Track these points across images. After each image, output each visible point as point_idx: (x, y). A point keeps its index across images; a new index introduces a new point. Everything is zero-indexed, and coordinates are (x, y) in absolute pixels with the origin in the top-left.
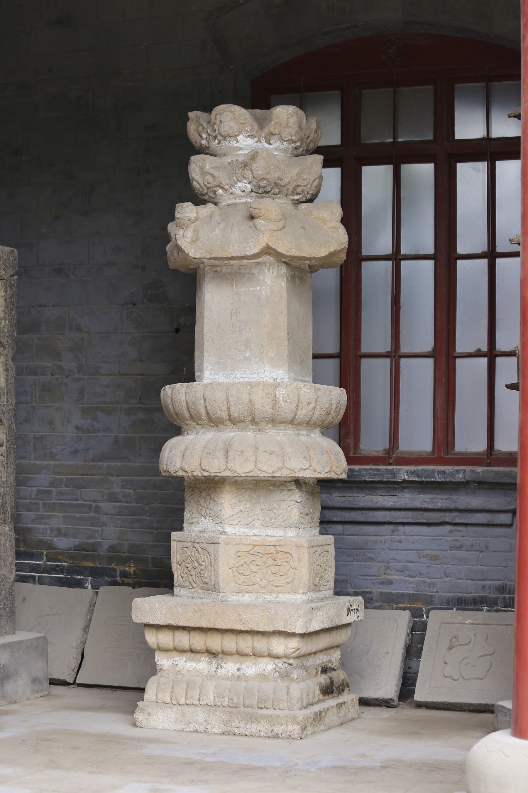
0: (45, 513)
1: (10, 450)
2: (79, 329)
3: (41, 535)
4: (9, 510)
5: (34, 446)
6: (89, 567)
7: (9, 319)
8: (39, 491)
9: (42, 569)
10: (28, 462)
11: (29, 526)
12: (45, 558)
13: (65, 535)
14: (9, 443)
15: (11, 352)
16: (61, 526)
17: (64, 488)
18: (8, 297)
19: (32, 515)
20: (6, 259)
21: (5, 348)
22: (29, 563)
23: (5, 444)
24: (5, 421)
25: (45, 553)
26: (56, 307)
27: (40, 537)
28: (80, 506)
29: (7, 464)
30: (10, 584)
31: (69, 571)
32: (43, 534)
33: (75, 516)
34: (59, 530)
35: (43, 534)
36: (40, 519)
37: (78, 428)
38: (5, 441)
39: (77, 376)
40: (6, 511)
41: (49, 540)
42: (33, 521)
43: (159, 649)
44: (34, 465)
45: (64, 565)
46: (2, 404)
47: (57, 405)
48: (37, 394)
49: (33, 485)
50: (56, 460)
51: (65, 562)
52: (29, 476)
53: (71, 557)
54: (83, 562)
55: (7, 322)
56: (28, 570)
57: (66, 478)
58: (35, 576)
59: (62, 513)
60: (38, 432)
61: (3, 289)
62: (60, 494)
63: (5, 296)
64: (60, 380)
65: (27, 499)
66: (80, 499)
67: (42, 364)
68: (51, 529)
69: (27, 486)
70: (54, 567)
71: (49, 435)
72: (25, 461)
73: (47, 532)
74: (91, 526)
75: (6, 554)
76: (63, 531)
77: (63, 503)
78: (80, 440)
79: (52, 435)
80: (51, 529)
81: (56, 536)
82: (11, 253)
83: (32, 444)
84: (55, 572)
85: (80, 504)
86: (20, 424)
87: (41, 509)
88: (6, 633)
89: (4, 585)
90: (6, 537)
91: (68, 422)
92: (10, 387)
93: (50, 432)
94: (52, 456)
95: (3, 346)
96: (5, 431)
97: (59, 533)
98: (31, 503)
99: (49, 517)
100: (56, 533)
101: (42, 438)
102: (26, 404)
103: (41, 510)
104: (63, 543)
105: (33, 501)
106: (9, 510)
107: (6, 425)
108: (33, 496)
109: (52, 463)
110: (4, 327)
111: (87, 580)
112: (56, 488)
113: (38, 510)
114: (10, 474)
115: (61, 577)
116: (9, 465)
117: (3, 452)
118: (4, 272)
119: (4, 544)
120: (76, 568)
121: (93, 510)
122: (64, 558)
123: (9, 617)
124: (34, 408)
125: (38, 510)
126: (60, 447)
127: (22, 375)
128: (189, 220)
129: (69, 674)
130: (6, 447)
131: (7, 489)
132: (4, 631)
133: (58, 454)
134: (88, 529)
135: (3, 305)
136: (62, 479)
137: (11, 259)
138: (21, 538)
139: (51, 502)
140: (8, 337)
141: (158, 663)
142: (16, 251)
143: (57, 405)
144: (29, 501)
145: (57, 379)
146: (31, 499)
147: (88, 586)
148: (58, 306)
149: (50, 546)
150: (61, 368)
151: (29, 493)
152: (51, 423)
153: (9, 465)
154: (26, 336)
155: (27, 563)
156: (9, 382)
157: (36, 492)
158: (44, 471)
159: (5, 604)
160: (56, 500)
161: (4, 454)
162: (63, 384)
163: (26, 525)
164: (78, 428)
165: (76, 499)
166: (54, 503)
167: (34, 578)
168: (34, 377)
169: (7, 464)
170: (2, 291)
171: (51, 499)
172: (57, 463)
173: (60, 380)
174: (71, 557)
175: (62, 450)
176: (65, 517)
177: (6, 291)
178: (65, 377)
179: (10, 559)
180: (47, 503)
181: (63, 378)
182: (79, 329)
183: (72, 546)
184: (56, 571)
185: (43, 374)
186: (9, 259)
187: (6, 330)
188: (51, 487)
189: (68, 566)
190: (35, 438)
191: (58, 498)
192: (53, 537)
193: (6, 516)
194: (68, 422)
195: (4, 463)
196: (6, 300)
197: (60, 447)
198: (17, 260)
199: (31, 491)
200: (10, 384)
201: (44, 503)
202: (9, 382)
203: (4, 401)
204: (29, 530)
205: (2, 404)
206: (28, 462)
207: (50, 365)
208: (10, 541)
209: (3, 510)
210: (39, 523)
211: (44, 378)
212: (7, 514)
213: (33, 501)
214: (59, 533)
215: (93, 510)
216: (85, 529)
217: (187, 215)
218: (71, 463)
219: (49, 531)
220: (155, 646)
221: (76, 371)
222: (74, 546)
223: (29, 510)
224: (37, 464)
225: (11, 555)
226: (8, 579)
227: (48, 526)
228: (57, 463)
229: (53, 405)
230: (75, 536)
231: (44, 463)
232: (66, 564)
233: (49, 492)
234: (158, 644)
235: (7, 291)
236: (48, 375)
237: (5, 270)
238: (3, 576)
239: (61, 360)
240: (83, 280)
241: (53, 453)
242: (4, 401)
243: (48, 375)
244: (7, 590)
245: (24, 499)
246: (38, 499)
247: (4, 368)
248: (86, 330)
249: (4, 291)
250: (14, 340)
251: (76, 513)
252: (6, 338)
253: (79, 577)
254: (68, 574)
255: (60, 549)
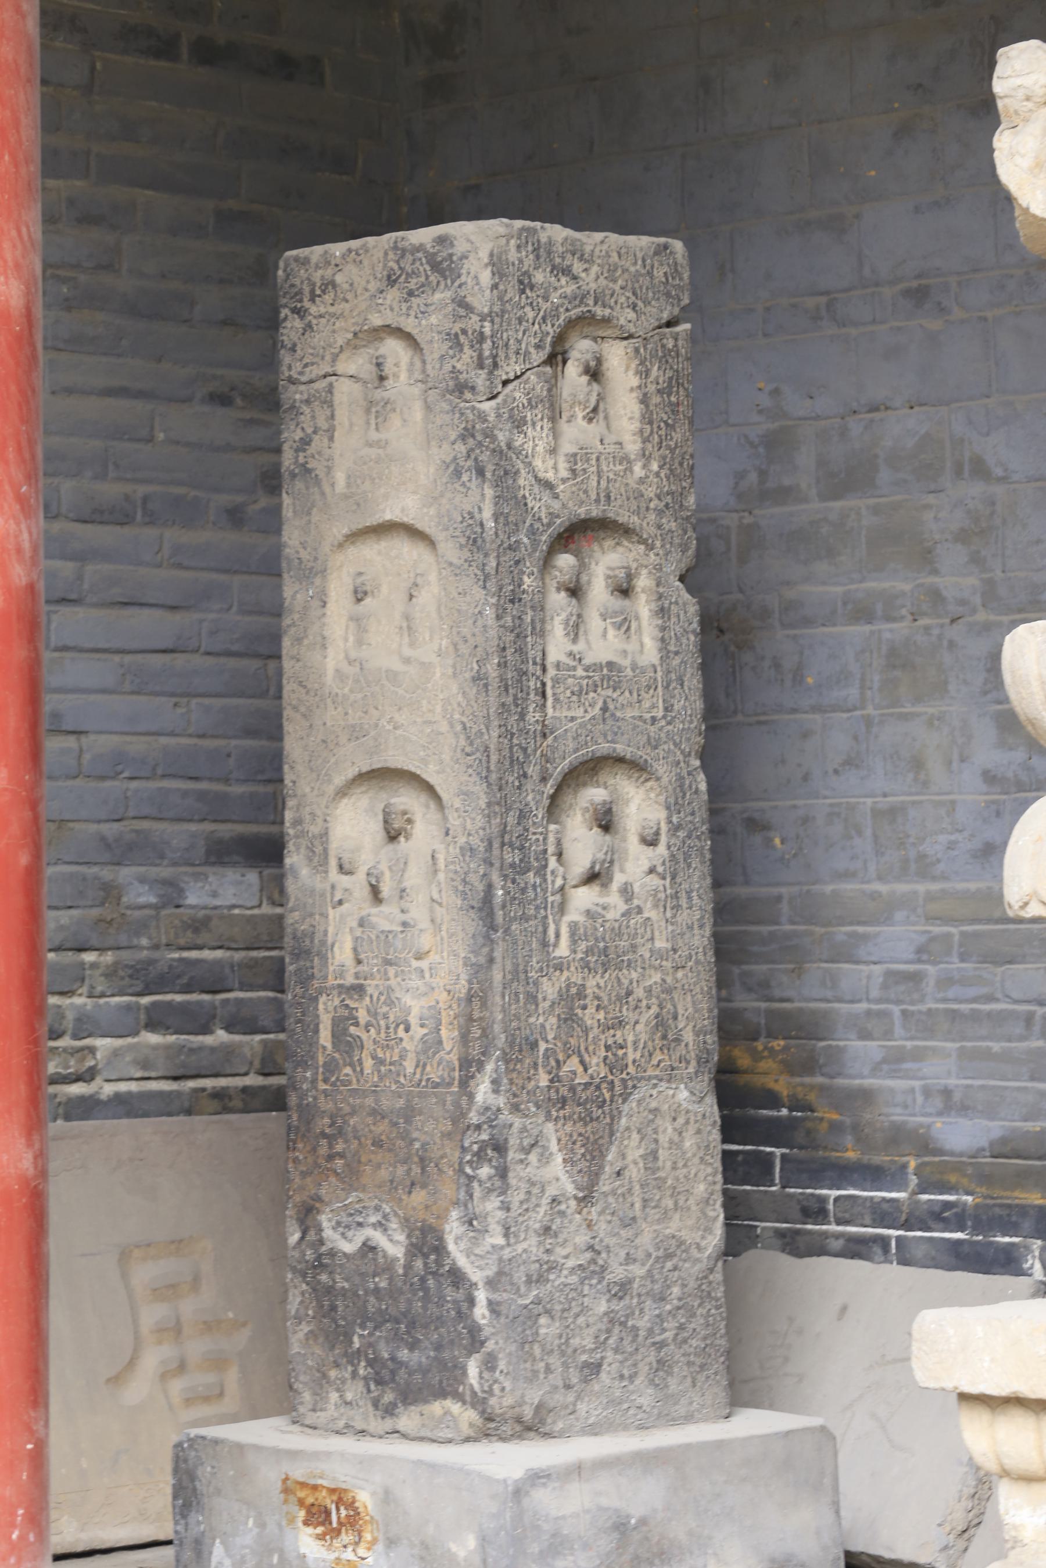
0: (909, 1044)
1: (687, 856)
2: (980, 470)
3: (899, 1110)
4: (688, 1036)
5: (876, 837)
6: (1035, 1206)
7: (664, 458)
8: (889, 974)
9: (904, 1217)
10: (858, 886)
11: (868, 1082)
12: (913, 1180)
13: (964, 1109)
14: (681, 834)
15: (676, 555)
16: (952, 1082)
17: (956, 965)
18: (652, 388)
19: (873, 1049)
20: (637, 275)
21: (651, 547)
22: (872, 1198)
23: (663, 839)
24: (661, 769)
25: (913, 1164)
26: (916, 409)
27: (897, 1116)
28: (999, 1018)
29: (676, 896)
30: (703, 1265)
31: (981, 1220)
32: (906, 1107)
33: (989, 1049)
34: (947, 1093)
35: (906, 1107)
36: (894, 1061)
37: (990, 778)
38: (664, 828)
39: (981, 616)
40: (678, 1040)
41: (921, 1126)
42: (876, 1069)
43: (1006, 1473)
44: (875, 896)
45: (965, 1204)
46: (648, 716)
47: (930, 710)
48: (877, 678)
49: (874, 959)
50: (934, 879)
51: (968, 1193)
52: (860, 929)
53: (985, 1178)
54: (1016, 1194)
55: (655, 466)
56: (868, 1220)
57: (963, 934)
58: (889, 1237)
59: (953, 1041)
60: (885, 795)
61: (633, 366)
62: (946, 982)
63: (639, 387)
64: (936, 632)
65: (859, 1001)
66: (999, 995)
67: (886, 585)
68: (927, 1092)
69: (857, 962)
70: (937, 1209)
71: (914, 803)
72: (849, 886)
73: (914, 1100)
74: (1032, 1079)
75: (681, 1172)
76: (957, 1096)
77: (954, 1011)
78: (998, 814)
79: (921, 802)
80: (927, 1092)
81: (940, 1114)
82: (656, 253)
83: (868, 832)
84: (941, 1225)
85: (1002, 1011)
86: (836, 772)
87: (898, 1030)
88: (689, 1418)
89: (675, 1268)
90: (681, 1120)
91: (963, 760)
92: (676, 661)
93: (917, 794)
94: (924, 868)
95: (643, 541)
96: (662, 798)
97: (950, 1103)
98: (869, 1013)
99: (918, 1055)
100: (938, 1103)
101: (893, 813)
102: (849, 711)
103: (896, 1036)
104: (961, 1135)
105: (874, 1007)
106: (688, 1036)
107: (665, 780)
108: (875, 993)
109: (921, 888)
110: (642, 481)
111: (1028, 1249)
112: (934, 963)
113: (888, 1034)
114: (690, 928)
115: (959, 1242)
116: (683, 902)
117: (658, 862)
118: (632, 315)
119: (671, 1142)
120: (997, 1210)
121: (1037, 1028)
122: (965, 1181)
123: (702, 1367)
124: (868, 721)
125: (888, 1034)
126: (943, 838)
127: (835, 625)
128: (1028, 99)
129: (946, 1548)
130: (669, 847)
131: (680, 974)
132: (681, 1409)
133: (939, 861)
134: (1026, 1088)
135: (637, 415)
136: (949, 935)
137: (659, 274)
138: (848, 1121)
139: (923, 1007)
140: (660, 513)
141: (1007, 1519)
142: (678, 246)
143: (930, 710)
144: (864, 1006)
145: (927, 629)
146: (868, 1000)
147: (1031, 1267)
148: (921, 405)
149: (925, 1145)
150: (936, 596)
151: (864, 981)
152: (917, 764)
153: (683, 902)
154: (838, 504)
155: (866, 1198)
156: (672, 648)
157: (881, 980)
158: (899, 915)
159: (681, 1327)
160: (938, 1001)
161: (660, 869)
162: (945, 643)
163: (857, 1082)
164: (990, 778)
165: (990, 998)
166: (930, 1010)
167: (883, 1242)
168: (867, 628)
169: (676, 896)
170: (631, 373)
171: (922, 1000)
172: (935, 887)
173: (936, 632)
174: (985, 1178)
175: (951, 846)
176: (962, 1053)
177: (644, 373)
178: (947, 621)
179: (702, 1187)
180: (913, 1013)
181: (942, 626)
182: (980, 470)
183: (984, 1143)
184: (944, 1220)
185: (889, 619)
186: (650, 274)
187: (650, 492)
188: (919, 961)
189: (977, 1206)
190: (877, 813)
191: (941, 995)
192: (929, 1115)
193: (676, 1056)
194: (963, 760)
195: (662, 896)
196: (644, 400)
197: (943, 838)
198: (686, 276)
199: (869, 977)
200: (677, 653)
201: (904, 1012)
202: (672, 648)
203: (654, 706)
204: (866, 1096)
205: (648, 716)
206: (858, 886)
207: (907, 587)
208: (699, 1132)
209: (664, 1037)
210: (893, 1074)
211: (891, 631)
212: (681, 1050)
213: (874, 1007)
214: (950, 1103)
215: (1037, 1028)
216: (1019, 1089)
217: (1018, 81)
218: (973, 886)
219: (920, 1099)
220: (990, 1465)
221: (977, 600)
222: (992, 1144)
223: (865, 1035)
224: (880, 894)
225: (701, 1175)
226: (694, 1253)
227: (917, 1084)
228: (935, 887)
229: (918, 709)
230: (990, 1113)
231: (902, 888)
232: (970, 1199)
233: (915, 978)
234: (998, 1458)
235: (648, 373)
236: (903, 618)
237: (634, 307)
238: (674, 1242)
239: (935, 572)
240: (985, 319)
241: (925, 856)
242: (654, 706)
243: (903, 618)
244: (692, 1284)
245: (852, 1002)
246: (887, 1001)
247: (654, 606)
248: (999, 472)
249: (637, 372)
250: (688, 518)
251: (991, 1040)
252: (652, 517)
253: (1007, 1239)
254: (976, 1229)
255: (952, 1154)
